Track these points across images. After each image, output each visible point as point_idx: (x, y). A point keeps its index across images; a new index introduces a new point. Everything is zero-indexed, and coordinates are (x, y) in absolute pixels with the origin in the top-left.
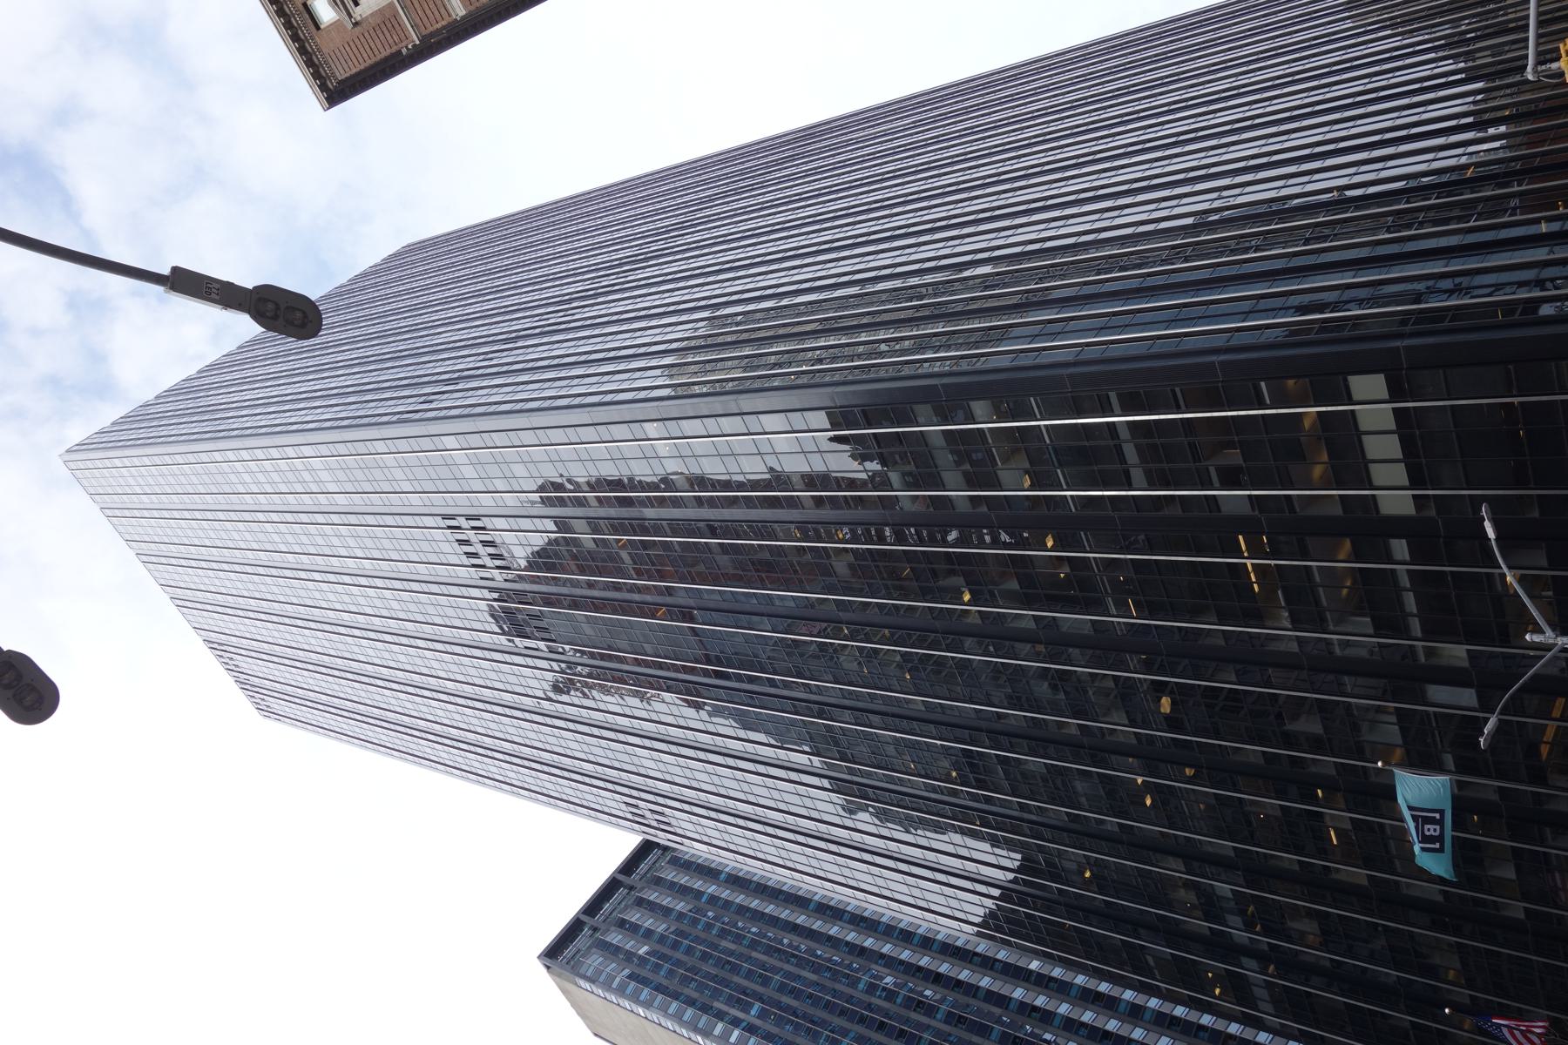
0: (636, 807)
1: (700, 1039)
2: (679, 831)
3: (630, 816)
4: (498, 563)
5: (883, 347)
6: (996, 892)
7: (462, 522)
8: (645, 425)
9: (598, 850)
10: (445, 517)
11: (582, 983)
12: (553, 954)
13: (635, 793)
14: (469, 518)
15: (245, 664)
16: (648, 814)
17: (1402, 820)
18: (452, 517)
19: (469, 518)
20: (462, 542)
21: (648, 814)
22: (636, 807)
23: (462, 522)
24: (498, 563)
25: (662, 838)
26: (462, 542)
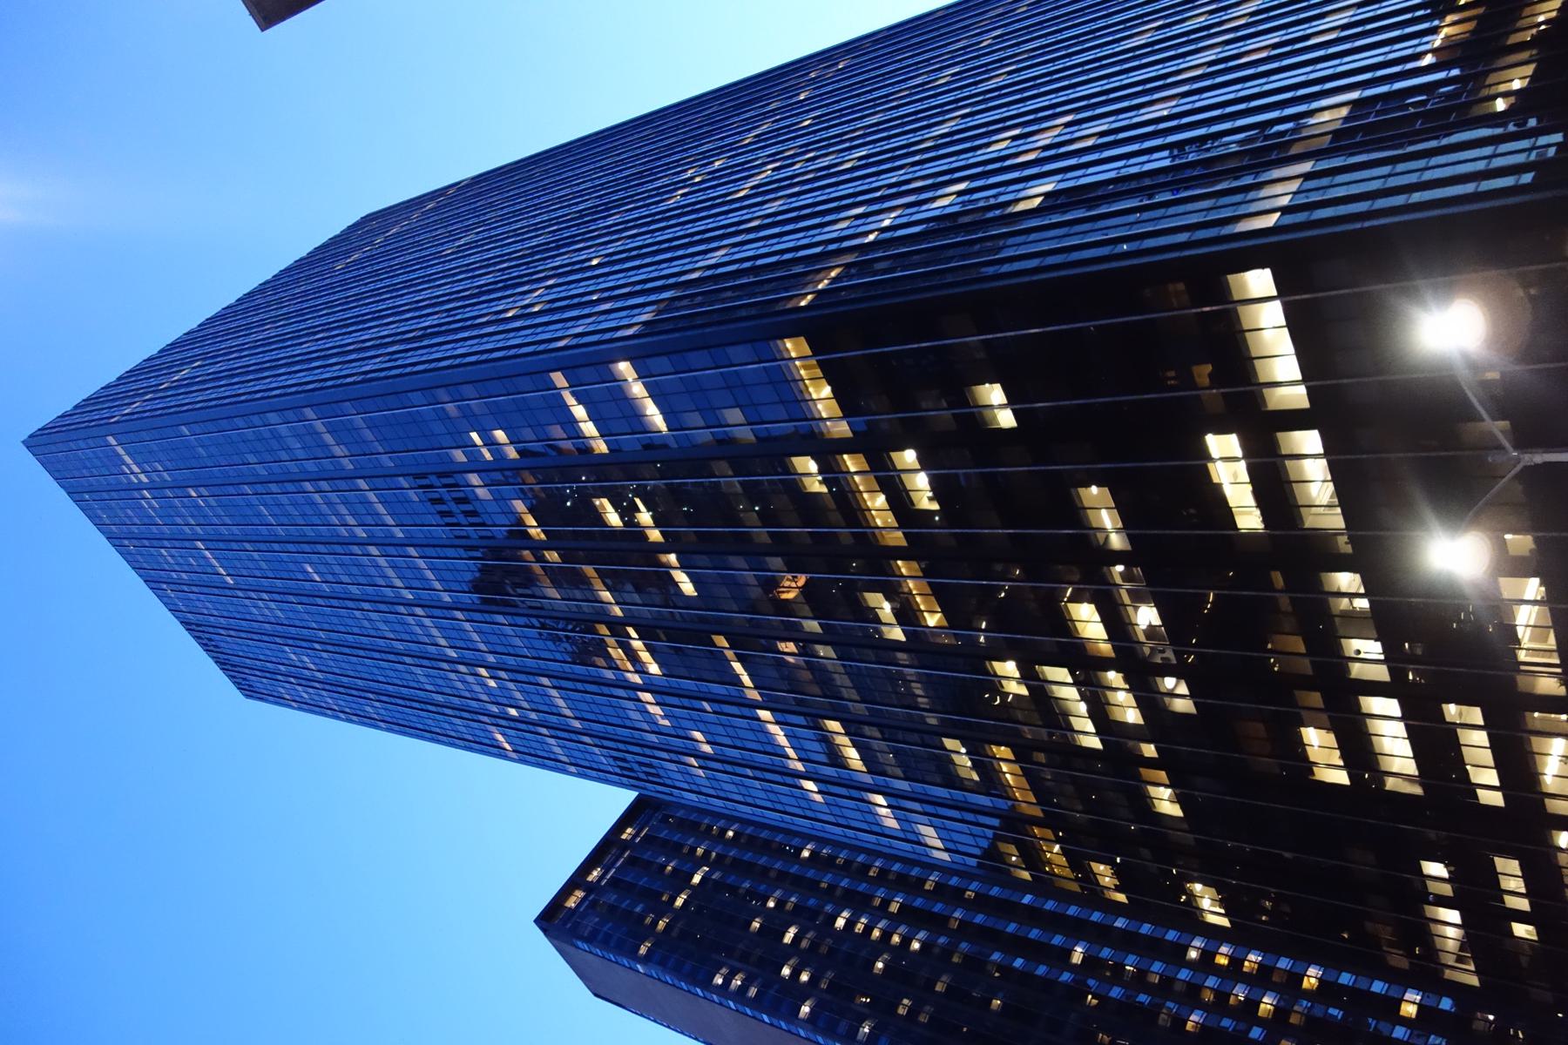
0: (624, 760)
1: (820, 1040)
2: (669, 782)
3: (618, 770)
4: (448, 520)
5: (729, 294)
6: (996, 822)
7: (433, 480)
8: (488, 384)
9: (591, 808)
10: (416, 476)
11: (579, 944)
12: (553, 920)
13: (621, 746)
14: (440, 475)
15: (228, 644)
16: (636, 767)
17: (649, 648)
18: (424, 476)
19: (440, 475)
20: (434, 501)
21: (636, 767)
22: (624, 760)
23: (433, 480)
24: (448, 520)
25: (652, 790)
26: (434, 501)
